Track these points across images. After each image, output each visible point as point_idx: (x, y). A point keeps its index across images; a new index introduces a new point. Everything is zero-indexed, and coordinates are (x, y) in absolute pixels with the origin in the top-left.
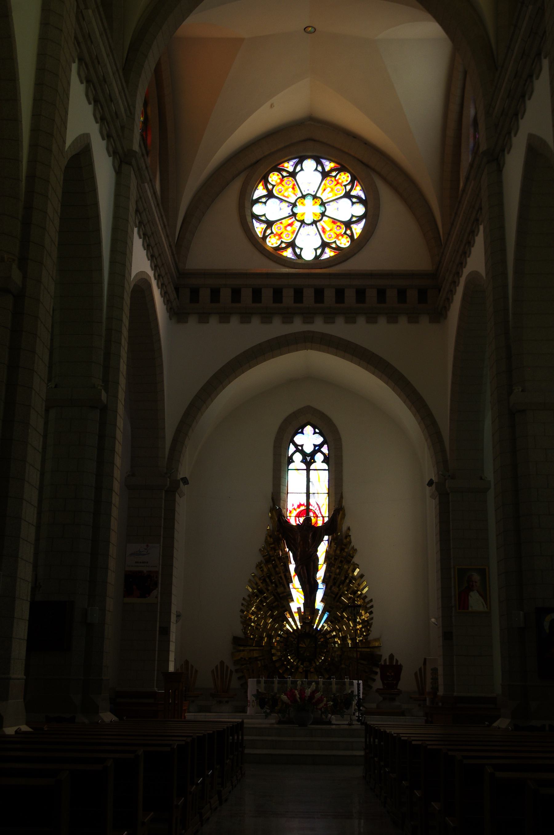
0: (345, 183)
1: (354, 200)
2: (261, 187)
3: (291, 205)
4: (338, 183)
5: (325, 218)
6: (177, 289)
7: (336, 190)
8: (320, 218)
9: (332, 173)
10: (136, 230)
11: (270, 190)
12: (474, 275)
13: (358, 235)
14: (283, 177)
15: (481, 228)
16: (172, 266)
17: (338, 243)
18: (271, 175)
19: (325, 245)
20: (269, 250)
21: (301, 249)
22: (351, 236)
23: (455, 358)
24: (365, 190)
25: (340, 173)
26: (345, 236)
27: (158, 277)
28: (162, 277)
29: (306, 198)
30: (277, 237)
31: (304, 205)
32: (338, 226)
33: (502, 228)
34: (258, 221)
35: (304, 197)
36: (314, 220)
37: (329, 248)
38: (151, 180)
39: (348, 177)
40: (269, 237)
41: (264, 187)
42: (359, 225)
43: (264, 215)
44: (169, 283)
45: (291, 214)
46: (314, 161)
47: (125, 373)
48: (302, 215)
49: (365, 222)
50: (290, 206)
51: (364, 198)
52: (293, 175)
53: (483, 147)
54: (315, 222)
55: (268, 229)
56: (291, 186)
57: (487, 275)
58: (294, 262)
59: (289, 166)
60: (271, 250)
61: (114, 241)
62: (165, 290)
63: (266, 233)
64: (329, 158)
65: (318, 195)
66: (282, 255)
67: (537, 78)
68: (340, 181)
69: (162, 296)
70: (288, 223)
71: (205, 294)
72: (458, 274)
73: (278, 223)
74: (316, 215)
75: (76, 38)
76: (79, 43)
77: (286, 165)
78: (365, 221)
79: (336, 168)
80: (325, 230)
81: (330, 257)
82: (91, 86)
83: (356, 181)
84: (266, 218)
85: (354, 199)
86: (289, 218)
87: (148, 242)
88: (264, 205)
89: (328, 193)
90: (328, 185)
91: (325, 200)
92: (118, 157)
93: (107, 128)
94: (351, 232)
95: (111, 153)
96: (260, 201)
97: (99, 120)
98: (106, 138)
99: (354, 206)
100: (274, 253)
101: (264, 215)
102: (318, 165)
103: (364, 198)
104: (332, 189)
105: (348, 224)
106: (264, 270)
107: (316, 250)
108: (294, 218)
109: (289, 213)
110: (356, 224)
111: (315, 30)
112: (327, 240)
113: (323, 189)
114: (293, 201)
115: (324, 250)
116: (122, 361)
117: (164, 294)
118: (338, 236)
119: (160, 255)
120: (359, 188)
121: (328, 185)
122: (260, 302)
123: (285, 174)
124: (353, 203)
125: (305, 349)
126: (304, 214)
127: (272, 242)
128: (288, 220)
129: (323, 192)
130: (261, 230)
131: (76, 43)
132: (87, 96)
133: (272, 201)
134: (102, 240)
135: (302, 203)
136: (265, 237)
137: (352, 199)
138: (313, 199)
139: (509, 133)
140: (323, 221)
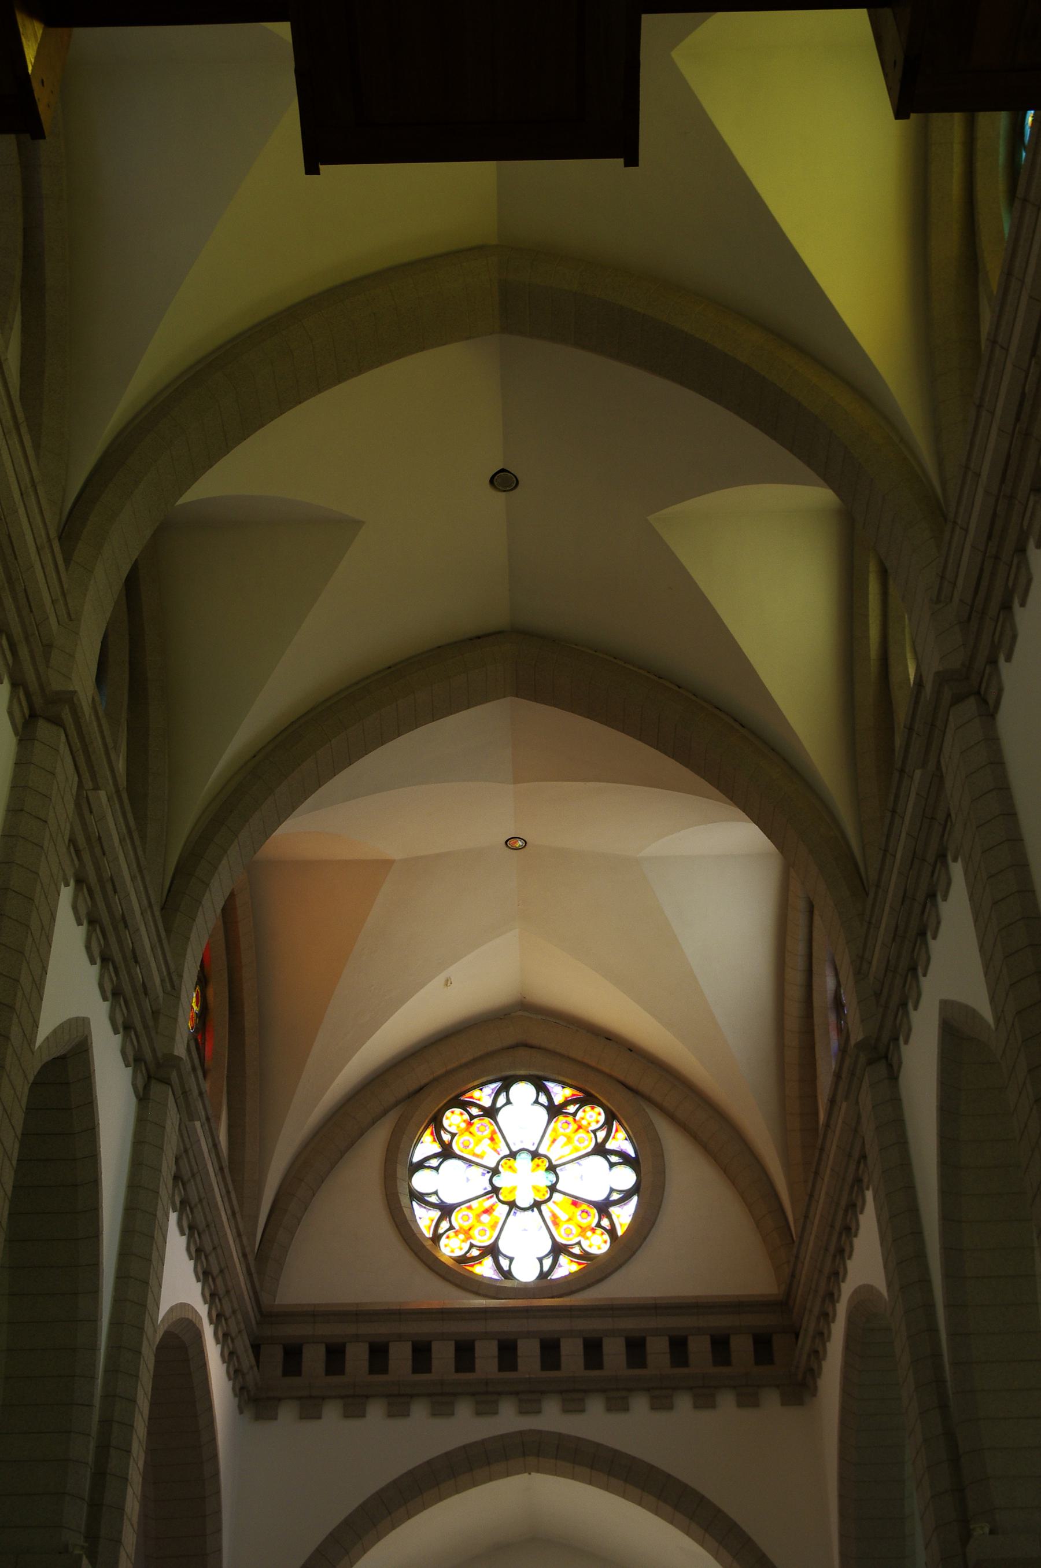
0: (595, 1126)
1: (614, 1159)
2: (427, 1137)
3: (488, 1172)
4: (580, 1127)
5: (556, 1195)
6: (256, 1348)
7: (578, 1141)
8: (547, 1196)
9: (568, 1107)
10: (173, 1217)
11: (447, 1143)
12: (865, 1293)
13: (625, 1228)
14: (472, 1117)
15: (869, 1195)
16: (246, 1297)
17: (585, 1245)
18: (448, 1113)
19: (558, 1250)
20: (445, 1262)
21: (511, 1260)
22: (612, 1232)
23: (842, 1480)
24: (633, 1138)
25: (583, 1108)
26: (599, 1231)
27: (218, 1318)
28: (226, 1320)
29: (518, 1157)
30: (462, 1236)
31: (514, 1170)
32: (583, 1211)
33: (909, 1188)
34: (423, 1205)
35: (513, 1155)
36: (535, 1200)
37: (566, 1256)
38: (208, 1119)
39: (600, 1114)
40: (445, 1236)
41: (434, 1138)
42: (626, 1207)
43: (436, 1193)
44: (240, 1332)
45: (489, 1188)
46: (532, 1086)
47: (135, 1519)
48: (511, 1192)
49: (638, 1202)
50: (487, 1174)
51: (633, 1155)
52: (491, 1113)
53: (857, 1035)
54: (537, 1205)
55: (443, 1220)
56: (488, 1134)
57: (889, 1284)
58: (496, 1286)
59: (484, 1096)
60: (450, 1263)
61: (128, 1232)
62: (231, 1346)
63: (440, 1229)
64: (561, 1078)
65: (541, 1151)
66: (471, 1272)
67: (945, 898)
68: (584, 1123)
69: (224, 1362)
70: (483, 1209)
71: (314, 1358)
72: (832, 1297)
73: (463, 1207)
74: (538, 1191)
75: (72, 841)
76: (78, 852)
77: (476, 1094)
78: (631, 1157)
79: (575, 1097)
80: (557, 1220)
81: (570, 1273)
82: (98, 929)
83: (614, 1123)
84: (440, 1199)
85: (613, 1157)
86: (485, 1197)
87: (198, 1244)
88: (434, 1172)
89: (562, 1147)
90: (561, 1131)
91: (556, 1161)
92: (143, 1068)
93: (125, 1011)
94: (610, 1222)
95: (131, 1059)
96: (427, 1165)
97: (109, 994)
98: (121, 1030)
99: (614, 1169)
100: (456, 1269)
101: (436, 1193)
102: (540, 1093)
103: (633, 1155)
104: (569, 1139)
105: (603, 1208)
106: (435, 1304)
107: (540, 1260)
108: (495, 1196)
109: (484, 1187)
110: (619, 1207)
111: (525, 845)
112: (562, 1240)
113: (552, 1139)
114: (493, 1165)
115: (558, 1260)
116: (130, 1491)
117: (229, 1357)
118: (583, 1230)
119: (221, 1271)
120: (621, 1135)
121: (561, 1131)
122: (429, 1370)
123: (475, 1111)
124: (612, 1165)
125: (525, 1472)
126: (514, 1189)
127: (451, 1247)
128: (484, 1200)
129: (550, 1146)
130: (428, 1223)
131: (72, 850)
132: (88, 948)
133: (451, 1164)
134: (102, 1231)
135: (510, 1167)
136: (436, 1238)
137: (608, 1156)
138: (532, 1159)
139: (904, 1005)
140: (554, 1202)
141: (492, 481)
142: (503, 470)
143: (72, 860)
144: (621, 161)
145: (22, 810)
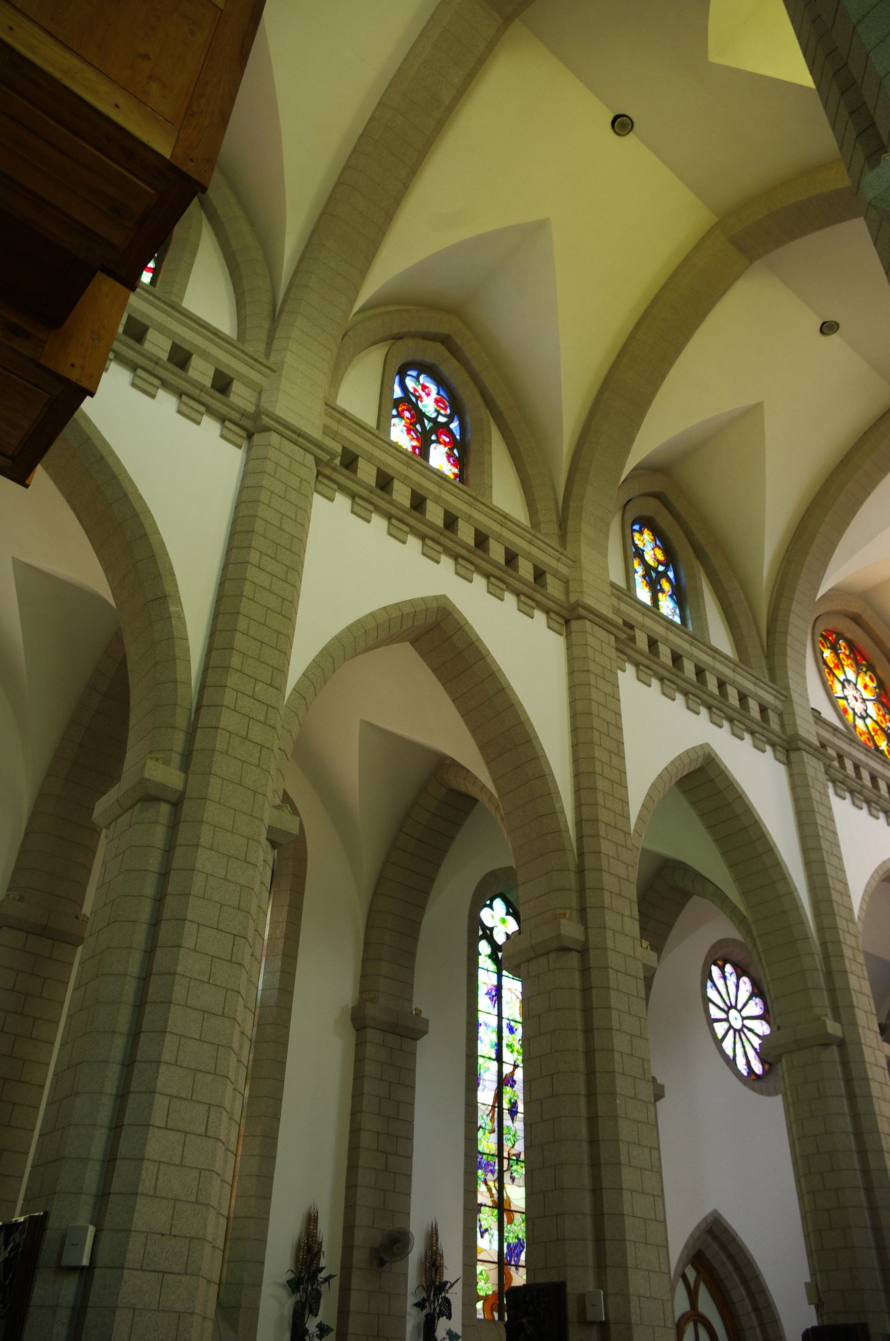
141: (821, 331)
142: (824, 323)
143: (646, 673)
144: (88, 398)
145: (574, 671)
